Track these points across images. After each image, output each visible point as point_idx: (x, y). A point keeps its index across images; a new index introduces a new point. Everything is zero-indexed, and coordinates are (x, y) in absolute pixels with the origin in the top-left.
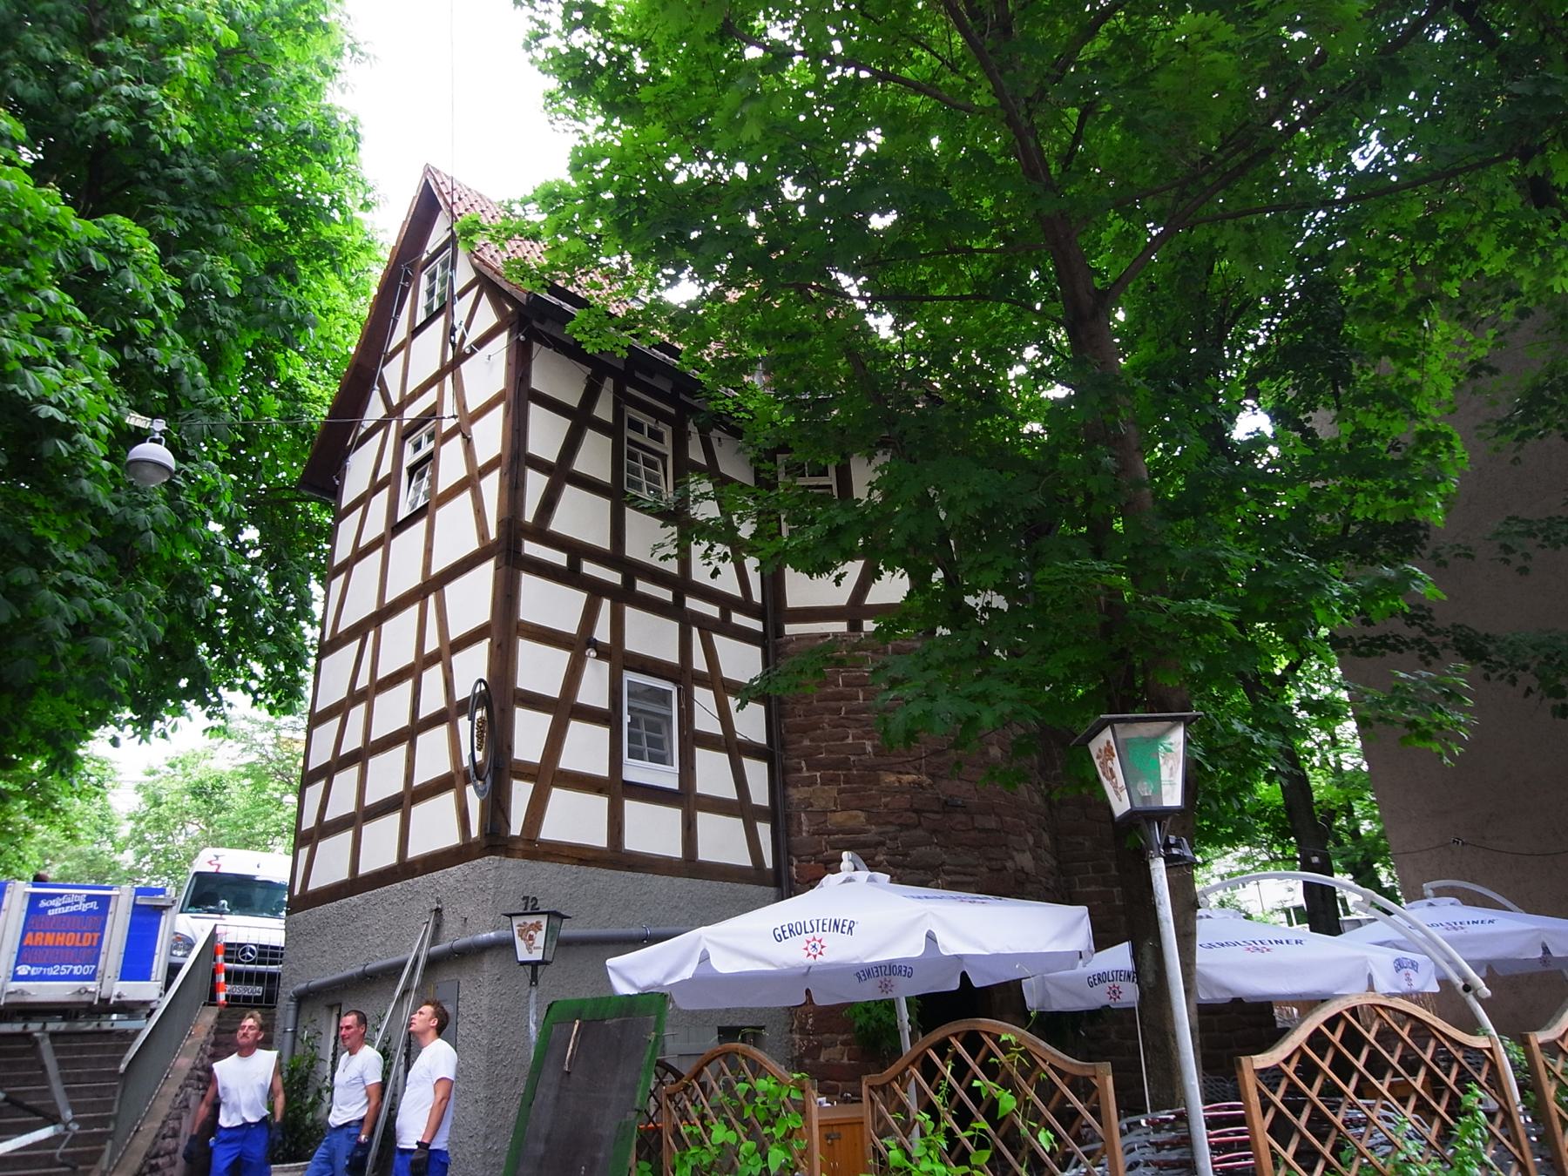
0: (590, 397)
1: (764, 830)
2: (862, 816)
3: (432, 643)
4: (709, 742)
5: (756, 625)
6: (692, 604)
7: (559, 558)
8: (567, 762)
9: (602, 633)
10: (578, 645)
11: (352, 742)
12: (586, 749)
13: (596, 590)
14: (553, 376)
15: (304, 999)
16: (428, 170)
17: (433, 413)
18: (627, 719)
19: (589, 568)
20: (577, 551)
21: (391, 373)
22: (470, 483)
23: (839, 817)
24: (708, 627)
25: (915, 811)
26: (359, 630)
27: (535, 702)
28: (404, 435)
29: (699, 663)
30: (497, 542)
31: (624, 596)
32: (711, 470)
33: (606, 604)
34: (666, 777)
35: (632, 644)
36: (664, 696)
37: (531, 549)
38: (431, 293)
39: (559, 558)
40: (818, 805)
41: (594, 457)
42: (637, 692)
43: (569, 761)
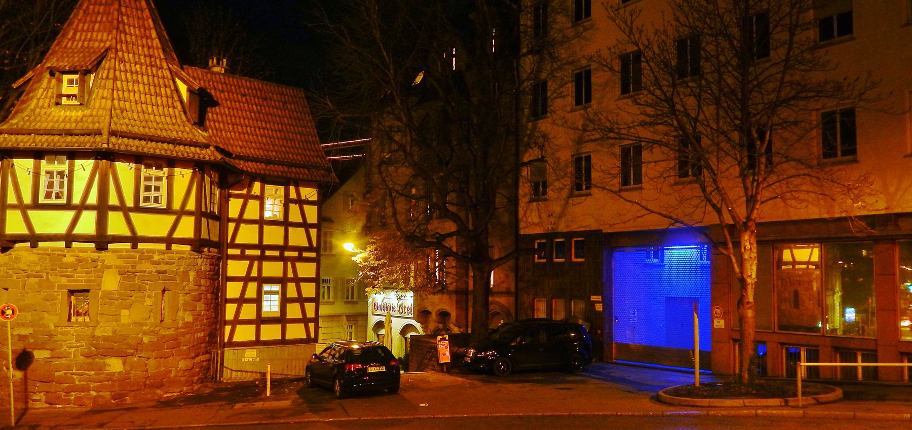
5: (313, 255)
8: (240, 284)
9: (290, 274)
20: (300, 249)
24: (294, 260)
31: (262, 258)
33: (256, 263)
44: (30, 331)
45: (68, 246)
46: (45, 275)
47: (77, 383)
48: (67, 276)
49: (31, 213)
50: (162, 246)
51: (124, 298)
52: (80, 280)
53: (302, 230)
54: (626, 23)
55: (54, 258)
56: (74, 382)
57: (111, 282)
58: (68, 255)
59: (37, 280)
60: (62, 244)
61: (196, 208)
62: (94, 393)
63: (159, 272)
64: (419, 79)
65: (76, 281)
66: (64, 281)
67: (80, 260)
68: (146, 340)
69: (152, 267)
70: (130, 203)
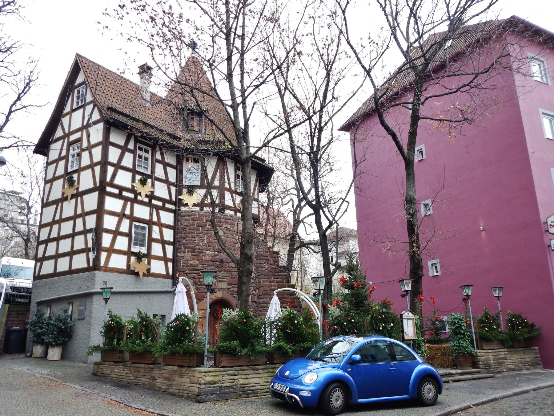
0: (127, 142)
1: (170, 265)
2: (198, 262)
3: (79, 211)
4: (156, 241)
5: (173, 207)
6: (154, 202)
7: (116, 191)
8: (116, 219)
9: (127, 212)
10: (121, 216)
11: (54, 234)
12: (122, 243)
14: (117, 138)
15: (39, 304)
16: (78, 55)
17: (79, 140)
18: (133, 235)
19: (125, 194)
20: (121, 189)
21: (65, 121)
22: (91, 166)
23: (191, 262)
24: (158, 208)
25: (213, 261)
26: (56, 202)
27: (108, 231)
28: (70, 144)
29: (155, 219)
30: (99, 187)
31: (135, 201)
32: (162, 162)
33: (129, 203)
35: (136, 214)
36: (144, 228)
37: (109, 189)
38: (78, 98)
39: (116, 191)
40: (186, 258)
41: (128, 160)
42: (136, 226)
43: (117, 247)
53: (130, 174)
54: (264, 49)
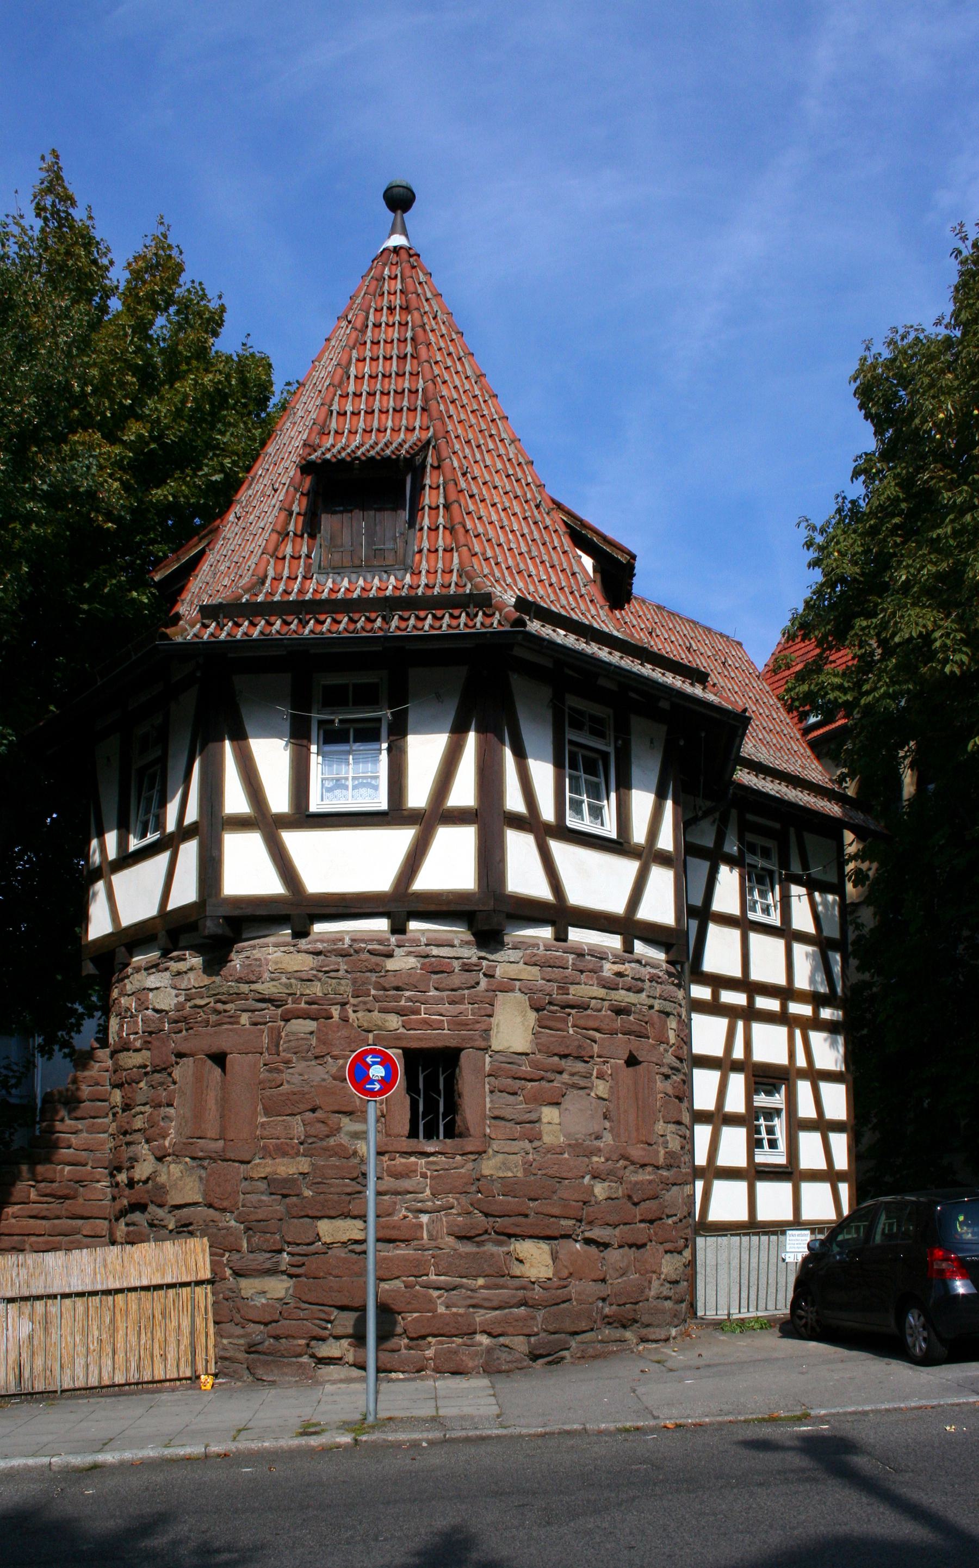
12: (734, 1148)
13: (730, 1012)
31: (751, 1014)
34: (778, 1158)
44: (304, 1165)
45: (398, 929)
46: (335, 1011)
47: (441, 1309)
48: (400, 1012)
49: (292, 840)
50: (614, 942)
51: (539, 1077)
52: (436, 1023)
55: (364, 960)
56: (434, 1311)
57: (513, 1029)
58: (398, 952)
59: (311, 1025)
60: (381, 925)
61: (795, 1086)
62: (484, 1340)
63: (619, 1011)
64: (52, 708)
65: (427, 1024)
66: (394, 1022)
67: (436, 969)
68: (600, 1190)
69: (601, 992)
70: (279, 800)
